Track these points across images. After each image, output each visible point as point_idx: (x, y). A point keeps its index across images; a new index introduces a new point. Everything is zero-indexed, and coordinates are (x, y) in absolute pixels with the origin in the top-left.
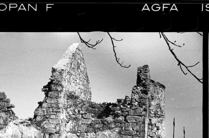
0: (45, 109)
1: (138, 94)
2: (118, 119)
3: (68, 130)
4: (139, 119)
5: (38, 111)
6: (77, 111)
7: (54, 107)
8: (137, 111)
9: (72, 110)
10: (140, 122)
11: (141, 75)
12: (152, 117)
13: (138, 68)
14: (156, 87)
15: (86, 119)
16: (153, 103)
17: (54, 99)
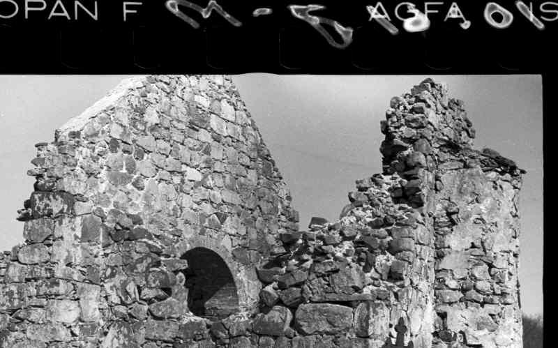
0: (14, 288)
1: (372, 205)
2: (266, 316)
4: (343, 316)
6: (131, 288)
8: (336, 281)
9: (118, 285)
10: (347, 329)
11: (393, 122)
12: (450, 304)
14: (469, 171)
15: (161, 318)
16: (455, 241)
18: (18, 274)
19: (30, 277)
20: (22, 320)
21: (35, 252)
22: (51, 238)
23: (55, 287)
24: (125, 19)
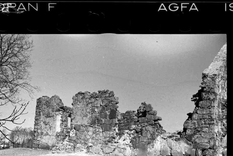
0: (195, 121)
7: (207, 119)
18: (197, 117)
19: (202, 118)
20: (199, 131)
21: (204, 110)
22: (210, 106)
23: (213, 121)
24: (49, 10)
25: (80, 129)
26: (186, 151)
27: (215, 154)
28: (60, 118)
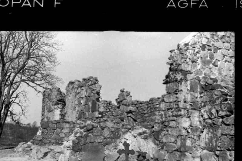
0: (163, 113)
3: (202, 146)
5: (155, 116)
6: (213, 111)
7: (174, 108)
13: (62, 79)
17: (173, 96)
18: (164, 107)
25: (49, 126)
26: (154, 153)
27: (182, 158)
28: (59, 113)
